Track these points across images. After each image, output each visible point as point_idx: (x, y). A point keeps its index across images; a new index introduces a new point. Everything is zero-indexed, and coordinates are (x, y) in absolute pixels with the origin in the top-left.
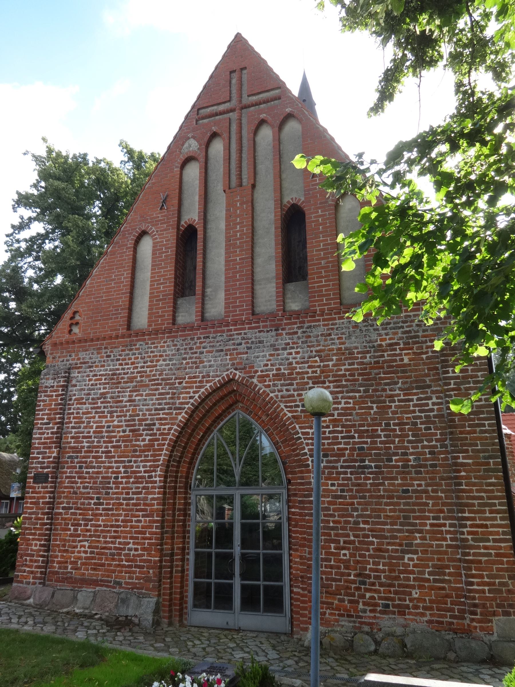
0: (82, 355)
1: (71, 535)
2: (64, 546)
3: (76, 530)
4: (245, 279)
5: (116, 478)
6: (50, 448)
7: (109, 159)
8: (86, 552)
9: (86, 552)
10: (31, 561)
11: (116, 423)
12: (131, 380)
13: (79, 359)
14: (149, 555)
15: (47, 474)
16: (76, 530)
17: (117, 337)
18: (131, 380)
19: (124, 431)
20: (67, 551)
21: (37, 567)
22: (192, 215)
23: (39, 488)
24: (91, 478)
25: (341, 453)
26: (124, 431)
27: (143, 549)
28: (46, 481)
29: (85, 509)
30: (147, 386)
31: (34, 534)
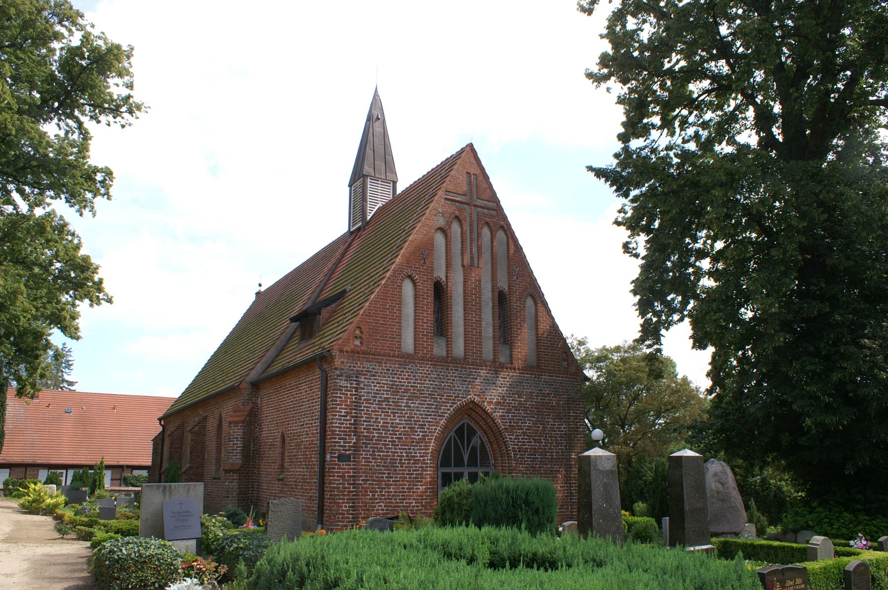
0: (367, 365)
1: (370, 499)
2: (365, 506)
3: (373, 495)
4: (472, 335)
5: (401, 460)
6: (350, 435)
7: (72, 4)
8: (383, 510)
9: (383, 510)
10: (343, 518)
11: (397, 421)
12: (406, 391)
13: (364, 367)
14: (426, 509)
15: (349, 455)
16: (373, 495)
17: (394, 356)
18: (406, 391)
19: (404, 428)
20: (368, 510)
21: (348, 522)
22: (440, 273)
23: (343, 465)
24: (381, 459)
25: (526, 450)
26: (404, 428)
27: (422, 506)
28: (349, 461)
29: (379, 481)
30: (419, 397)
31: (344, 499)
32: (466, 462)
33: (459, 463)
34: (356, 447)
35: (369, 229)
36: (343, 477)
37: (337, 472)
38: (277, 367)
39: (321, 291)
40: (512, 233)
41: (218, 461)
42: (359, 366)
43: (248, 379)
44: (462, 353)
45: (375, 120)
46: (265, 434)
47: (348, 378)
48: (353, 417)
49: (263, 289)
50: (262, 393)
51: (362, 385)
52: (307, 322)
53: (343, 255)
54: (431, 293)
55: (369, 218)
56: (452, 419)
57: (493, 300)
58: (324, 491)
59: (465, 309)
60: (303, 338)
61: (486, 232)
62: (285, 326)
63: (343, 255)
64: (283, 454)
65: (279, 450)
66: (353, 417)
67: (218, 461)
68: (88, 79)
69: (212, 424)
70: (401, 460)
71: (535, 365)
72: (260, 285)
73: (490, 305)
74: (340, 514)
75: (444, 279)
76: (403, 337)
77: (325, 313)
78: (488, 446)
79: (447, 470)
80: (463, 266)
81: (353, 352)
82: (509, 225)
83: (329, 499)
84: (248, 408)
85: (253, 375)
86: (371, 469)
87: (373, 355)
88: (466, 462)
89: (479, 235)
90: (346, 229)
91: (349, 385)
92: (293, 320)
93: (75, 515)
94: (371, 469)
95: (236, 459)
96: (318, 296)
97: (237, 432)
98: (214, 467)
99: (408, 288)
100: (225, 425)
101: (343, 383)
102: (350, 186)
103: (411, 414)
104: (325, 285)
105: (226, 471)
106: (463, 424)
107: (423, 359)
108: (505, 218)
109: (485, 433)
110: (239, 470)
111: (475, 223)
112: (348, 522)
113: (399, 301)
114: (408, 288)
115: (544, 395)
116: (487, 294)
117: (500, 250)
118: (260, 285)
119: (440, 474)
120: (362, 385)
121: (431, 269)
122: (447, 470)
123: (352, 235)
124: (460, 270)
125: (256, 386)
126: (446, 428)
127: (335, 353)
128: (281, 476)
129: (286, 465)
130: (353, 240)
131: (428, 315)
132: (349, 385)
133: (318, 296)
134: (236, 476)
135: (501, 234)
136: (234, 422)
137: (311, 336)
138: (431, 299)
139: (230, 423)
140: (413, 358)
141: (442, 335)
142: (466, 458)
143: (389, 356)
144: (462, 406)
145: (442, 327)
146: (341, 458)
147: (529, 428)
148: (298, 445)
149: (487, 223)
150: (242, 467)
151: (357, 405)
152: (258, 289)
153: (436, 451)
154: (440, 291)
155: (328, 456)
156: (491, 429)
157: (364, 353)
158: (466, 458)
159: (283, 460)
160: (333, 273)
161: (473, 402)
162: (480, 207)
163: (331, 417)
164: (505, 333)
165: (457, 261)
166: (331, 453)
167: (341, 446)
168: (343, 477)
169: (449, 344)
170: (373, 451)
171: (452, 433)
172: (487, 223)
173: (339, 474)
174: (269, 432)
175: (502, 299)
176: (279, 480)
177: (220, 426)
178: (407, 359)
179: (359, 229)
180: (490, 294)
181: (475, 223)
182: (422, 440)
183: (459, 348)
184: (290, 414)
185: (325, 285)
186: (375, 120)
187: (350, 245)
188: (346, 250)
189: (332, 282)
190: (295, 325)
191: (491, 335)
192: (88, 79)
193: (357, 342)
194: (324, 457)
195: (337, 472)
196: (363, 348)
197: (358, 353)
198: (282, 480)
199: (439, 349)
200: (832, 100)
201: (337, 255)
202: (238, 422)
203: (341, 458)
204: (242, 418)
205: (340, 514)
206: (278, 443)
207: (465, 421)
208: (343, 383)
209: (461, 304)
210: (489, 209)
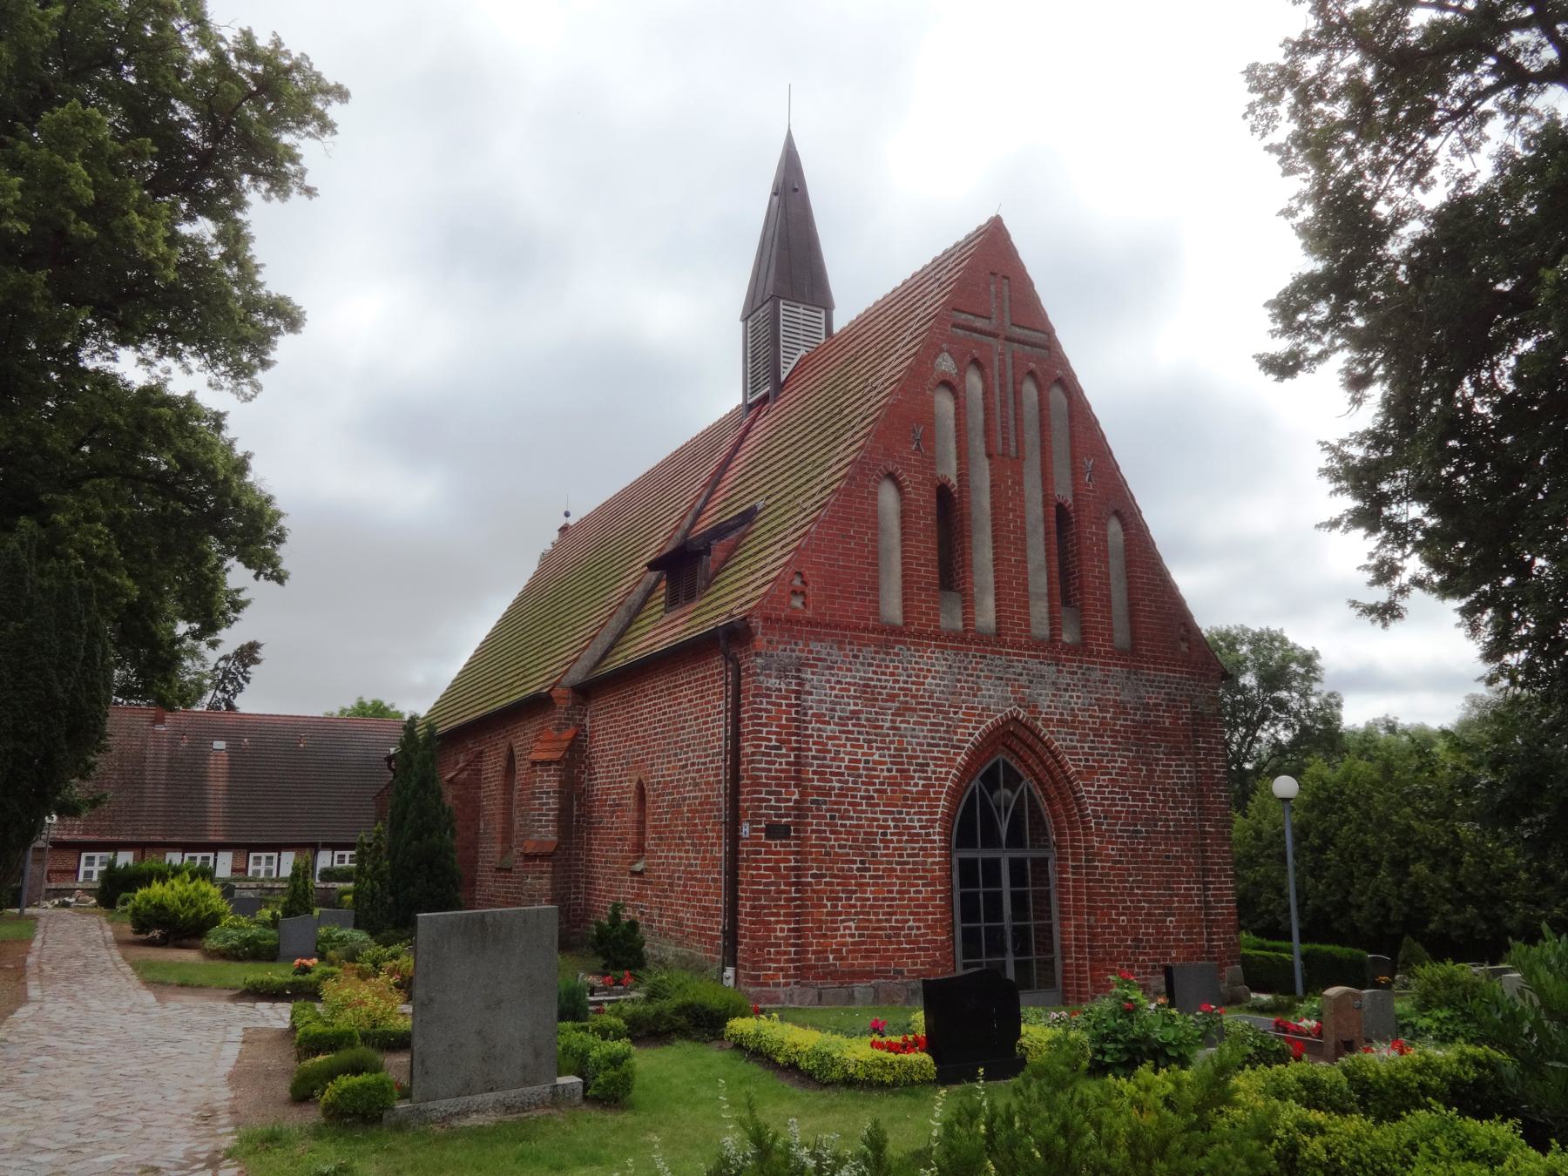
1: (828, 914)
2: (820, 929)
5: (884, 834)
8: (852, 936)
9: (852, 936)
10: (777, 953)
11: (876, 757)
12: (892, 698)
13: (810, 652)
14: (935, 934)
15: (787, 826)
16: (835, 906)
17: (866, 629)
18: (892, 698)
19: (889, 770)
20: (825, 936)
21: (787, 961)
22: (949, 470)
24: (848, 833)
26: (889, 770)
27: (927, 927)
28: (788, 837)
29: (845, 877)
30: (914, 710)
31: (778, 915)
32: (1004, 837)
33: (991, 840)
34: (800, 810)
35: (787, 397)
36: (775, 869)
37: (765, 861)
38: (618, 661)
39: (699, 513)
40: (1080, 392)
41: (507, 836)
42: (798, 651)
43: (566, 681)
44: (993, 625)
45: (790, 192)
46: (601, 782)
47: (782, 673)
48: (793, 749)
49: (572, 521)
50: (593, 706)
51: (807, 688)
52: (683, 568)
53: (736, 448)
54: (932, 506)
55: (783, 378)
56: (977, 754)
57: (1046, 521)
58: (737, 898)
59: (995, 539)
60: (673, 602)
61: (1029, 390)
62: (635, 574)
63: (736, 448)
64: (641, 823)
65: (631, 815)
66: (793, 749)
67: (507, 836)
68: (256, 115)
69: (493, 766)
70: (884, 834)
71: (1127, 647)
72: (567, 514)
73: (1041, 530)
74: (772, 945)
75: (954, 480)
76: (882, 592)
77: (718, 549)
78: (1043, 805)
79: (968, 854)
80: (989, 456)
81: (788, 621)
82: (1072, 377)
83: (747, 914)
84: (568, 734)
85: (577, 675)
86: (827, 854)
87: (827, 626)
88: (1004, 837)
89: (1017, 394)
90: (740, 401)
91: (783, 687)
92: (652, 566)
93: (627, 1056)
94: (827, 854)
95: (547, 833)
96: (693, 525)
97: (549, 781)
98: (498, 848)
99: (888, 498)
100: (522, 767)
101: (773, 682)
102: (745, 319)
103: (900, 742)
104: (706, 503)
105: (528, 857)
106: (996, 764)
107: (920, 635)
108: (1063, 362)
109: (1039, 781)
110: (553, 854)
111: (1010, 373)
112: (787, 961)
113: (872, 520)
114: (888, 498)
115: (1146, 706)
116: (1035, 511)
117: (1059, 426)
118: (567, 514)
119: (955, 862)
120: (807, 688)
121: (930, 462)
122: (968, 854)
123: (754, 408)
124: (985, 464)
125: (587, 691)
126: (966, 770)
127: (757, 623)
128: (639, 867)
129: (649, 844)
130: (754, 420)
131: (927, 547)
132: (783, 687)
133: (693, 525)
134: (547, 866)
135: (1057, 395)
136: (543, 763)
137: (691, 596)
138: (931, 520)
139: (534, 763)
140: (902, 633)
141: (951, 589)
142: (1004, 829)
143: (856, 628)
144: (996, 728)
145: (950, 570)
146: (775, 831)
147: (1122, 772)
148: (675, 807)
149: (1031, 373)
150: (558, 847)
151: (798, 724)
152: (562, 521)
153: (949, 816)
154: (948, 508)
155: (745, 830)
156: (1050, 773)
157: (809, 623)
158: (1004, 829)
159: (641, 834)
160: (718, 482)
161: (1015, 719)
162: (1019, 342)
163: (749, 750)
164: (1068, 585)
165: (978, 445)
166: (752, 823)
167: (771, 808)
168: (775, 869)
169: (968, 605)
170: (832, 818)
171: (976, 783)
172: (1031, 373)
173: (766, 864)
174: (610, 778)
175: (1062, 520)
176: (634, 873)
177: (510, 770)
178: (889, 636)
179: (765, 399)
180: (1039, 511)
181: (1010, 373)
182: (923, 794)
183: (986, 616)
184: (669, 746)
185: (706, 503)
186: (790, 192)
187: (748, 430)
188: (742, 439)
189: (719, 497)
190: (653, 576)
191: (1045, 590)
192: (256, 115)
193: (797, 602)
194: (737, 830)
195: (765, 861)
196: (809, 613)
197: (798, 622)
198: (640, 873)
199: (951, 620)
200: (1531, 211)
201: (726, 448)
202: (550, 763)
203: (775, 831)
204: (557, 755)
205: (772, 945)
206: (630, 800)
207: (1000, 756)
208: (773, 682)
209: (988, 530)
210: (1034, 345)
